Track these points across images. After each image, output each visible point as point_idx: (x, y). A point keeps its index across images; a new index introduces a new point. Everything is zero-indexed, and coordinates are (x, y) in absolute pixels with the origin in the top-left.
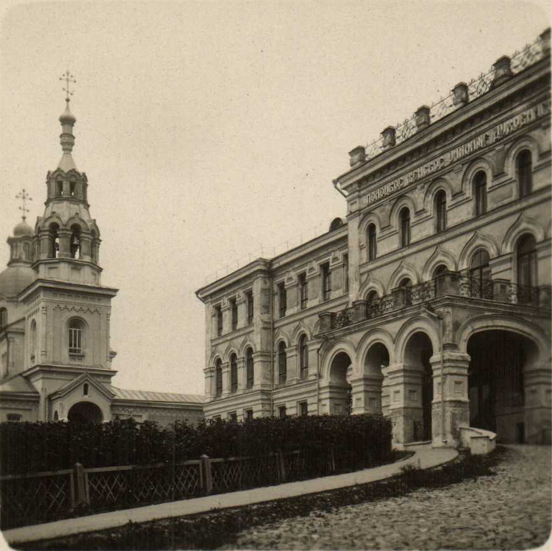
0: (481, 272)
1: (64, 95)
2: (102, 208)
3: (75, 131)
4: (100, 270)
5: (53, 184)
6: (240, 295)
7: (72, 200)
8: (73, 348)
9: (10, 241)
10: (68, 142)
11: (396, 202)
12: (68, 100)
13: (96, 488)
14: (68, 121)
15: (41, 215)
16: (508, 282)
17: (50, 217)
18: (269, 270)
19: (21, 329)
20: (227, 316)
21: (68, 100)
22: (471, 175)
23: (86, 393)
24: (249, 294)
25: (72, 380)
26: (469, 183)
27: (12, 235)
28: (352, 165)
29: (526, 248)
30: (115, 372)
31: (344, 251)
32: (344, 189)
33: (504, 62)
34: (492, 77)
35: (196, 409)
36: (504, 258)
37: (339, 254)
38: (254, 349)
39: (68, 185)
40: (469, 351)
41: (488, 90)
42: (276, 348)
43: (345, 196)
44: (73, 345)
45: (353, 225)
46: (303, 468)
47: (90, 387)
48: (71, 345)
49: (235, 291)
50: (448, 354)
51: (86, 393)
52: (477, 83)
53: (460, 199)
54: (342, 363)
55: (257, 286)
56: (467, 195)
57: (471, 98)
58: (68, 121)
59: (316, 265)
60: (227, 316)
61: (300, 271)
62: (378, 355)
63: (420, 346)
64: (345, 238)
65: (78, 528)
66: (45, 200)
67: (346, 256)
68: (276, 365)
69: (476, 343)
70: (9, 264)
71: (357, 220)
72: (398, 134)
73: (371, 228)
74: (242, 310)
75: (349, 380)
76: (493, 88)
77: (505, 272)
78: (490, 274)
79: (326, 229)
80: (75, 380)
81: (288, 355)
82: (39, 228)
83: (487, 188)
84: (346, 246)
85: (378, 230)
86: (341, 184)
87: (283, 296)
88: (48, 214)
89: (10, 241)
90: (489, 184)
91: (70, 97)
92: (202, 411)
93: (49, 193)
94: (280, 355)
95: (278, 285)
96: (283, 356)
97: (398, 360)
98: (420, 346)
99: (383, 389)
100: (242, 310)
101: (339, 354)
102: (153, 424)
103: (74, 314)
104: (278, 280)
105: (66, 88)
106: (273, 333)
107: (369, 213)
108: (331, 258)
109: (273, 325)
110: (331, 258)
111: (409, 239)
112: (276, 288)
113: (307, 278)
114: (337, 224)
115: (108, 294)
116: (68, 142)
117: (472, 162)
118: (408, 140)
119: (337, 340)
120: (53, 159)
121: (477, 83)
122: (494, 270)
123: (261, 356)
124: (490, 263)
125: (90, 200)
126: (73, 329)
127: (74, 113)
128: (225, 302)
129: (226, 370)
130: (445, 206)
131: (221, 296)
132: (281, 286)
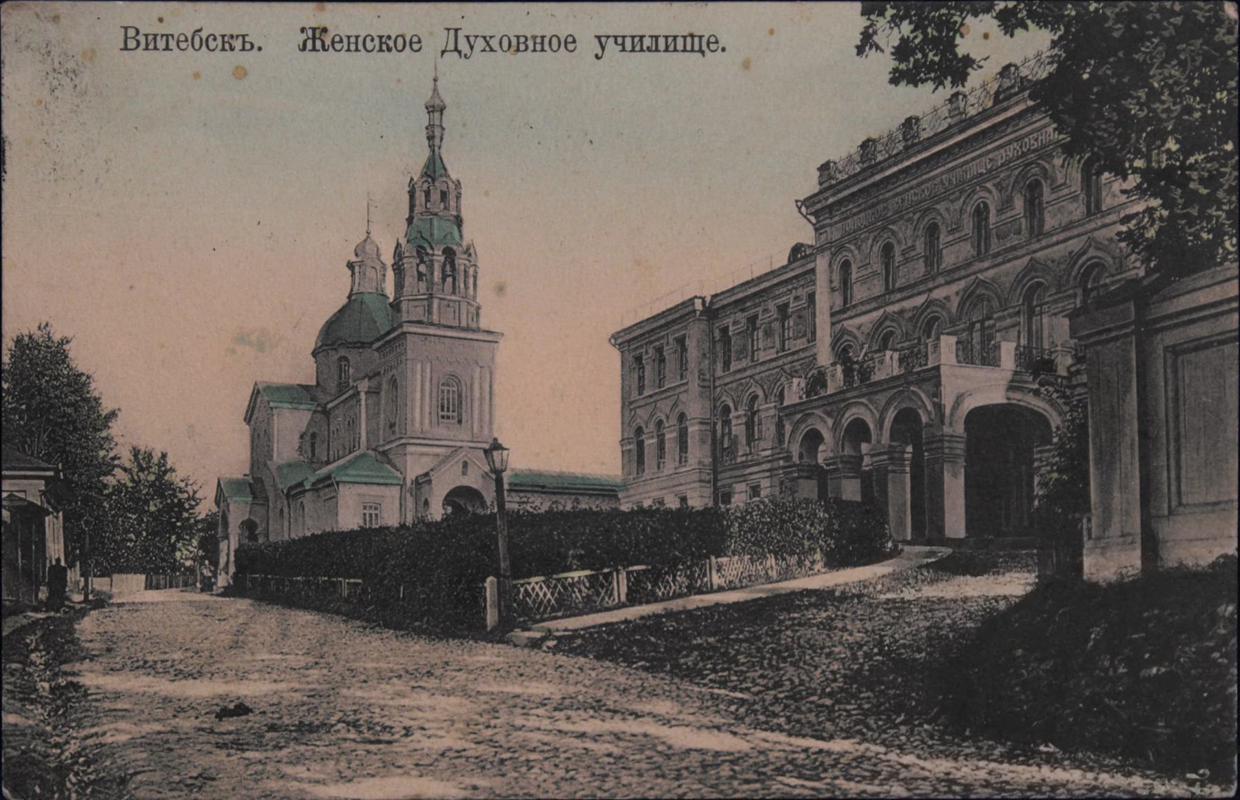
14: (435, 109)
18: (712, 311)
21: (435, 80)
22: (880, 243)
24: (681, 341)
26: (1079, 162)
28: (821, 184)
31: (808, 290)
32: (811, 214)
35: (608, 491)
37: (803, 292)
45: (821, 263)
46: (853, 247)
49: (686, 327)
52: (978, 93)
53: (957, 235)
56: (918, 250)
59: (772, 306)
61: (780, 301)
64: (813, 271)
65: (833, 290)
67: (811, 297)
84: (813, 282)
85: (854, 268)
86: (807, 207)
92: (616, 496)
107: (841, 248)
108: (791, 297)
110: (760, 309)
111: (894, 281)
112: (717, 334)
113: (790, 310)
114: (797, 251)
123: (701, 423)
129: (651, 441)
132: (725, 330)
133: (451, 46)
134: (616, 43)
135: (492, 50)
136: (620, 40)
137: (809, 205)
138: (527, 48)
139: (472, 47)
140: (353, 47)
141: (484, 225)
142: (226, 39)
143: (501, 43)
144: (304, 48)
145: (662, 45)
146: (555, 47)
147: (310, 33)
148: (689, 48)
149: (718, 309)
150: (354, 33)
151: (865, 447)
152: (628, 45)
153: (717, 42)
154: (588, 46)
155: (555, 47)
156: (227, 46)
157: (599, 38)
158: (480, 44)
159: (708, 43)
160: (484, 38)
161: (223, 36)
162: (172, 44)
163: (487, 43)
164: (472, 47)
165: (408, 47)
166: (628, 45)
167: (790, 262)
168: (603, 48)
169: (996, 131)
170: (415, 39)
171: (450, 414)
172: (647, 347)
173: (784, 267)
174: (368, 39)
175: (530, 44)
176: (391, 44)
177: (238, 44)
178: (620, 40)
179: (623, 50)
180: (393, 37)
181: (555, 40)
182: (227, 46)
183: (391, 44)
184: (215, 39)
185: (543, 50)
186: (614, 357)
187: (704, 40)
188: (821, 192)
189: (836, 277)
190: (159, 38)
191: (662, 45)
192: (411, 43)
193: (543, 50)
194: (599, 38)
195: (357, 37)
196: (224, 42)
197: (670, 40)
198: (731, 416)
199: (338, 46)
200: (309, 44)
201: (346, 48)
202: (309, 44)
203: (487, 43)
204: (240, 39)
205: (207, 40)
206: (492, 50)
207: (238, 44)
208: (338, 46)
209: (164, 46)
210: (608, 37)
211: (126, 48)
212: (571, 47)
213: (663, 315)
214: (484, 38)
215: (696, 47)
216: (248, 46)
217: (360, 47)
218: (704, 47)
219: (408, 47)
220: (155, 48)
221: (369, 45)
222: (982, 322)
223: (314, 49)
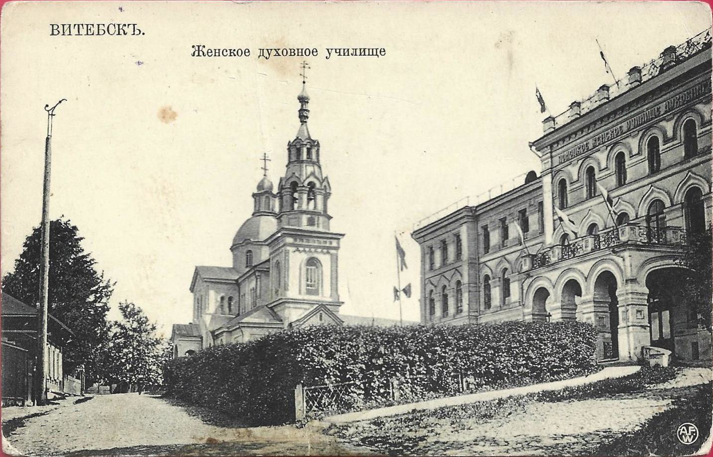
0: (657, 217)
2: (332, 163)
3: (309, 106)
4: (330, 218)
5: (294, 151)
6: (450, 238)
7: (310, 161)
8: (309, 283)
10: (303, 116)
12: (304, 82)
13: (311, 403)
15: (283, 175)
17: (291, 177)
18: (473, 214)
19: (267, 268)
20: (438, 255)
24: (458, 237)
27: (256, 191)
29: (693, 202)
33: (671, 50)
34: (661, 62)
36: (676, 207)
39: (302, 150)
40: (648, 285)
41: (657, 74)
44: (309, 280)
45: (547, 180)
48: (307, 281)
50: (629, 287)
51: (321, 319)
54: (542, 294)
57: (644, 79)
58: (303, 100)
60: (438, 255)
63: (607, 281)
68: (482, 293)
69: (653, 280)
72: (644, 72)
74: (452, 249)
77: (677, 220)
78: (666, 220)
79: (521, 181)
83: (660, 150)
88: (290, 174)
89: (254, 195)
93: (290, 157)
94: (485, 286)
96: (487, 287)
97: (589, 291)
98: (607, 281)
100: (452, 249)
102: (237, 344)
104: (481, 224)
105: (302, 74)
108: (528, 205)
112: (481, 231)
115: (338, 237)
116: (303, 116)
117: (648, 128)
118: (591, 111)
120: (291, 130)
121: (649, 67)
122: (668, 217)
124: (665, 211)
125: (322, 162)
126: (309, 267)
127: (309, 93)
128: (436, 243)
130: (624, 165)
131: (435, 236)
134: (336, 52)
135: (279, 55)
136: (338, 52)
138: (295, 54)
139: (269, 54)
140: (217, 54)
142: (232, 51)
144: (194, 55)
145: (358, 53)
146: (307, 54)
147: (197, 48)
148: (371, 54)
151: (577, 299)
152: (342, 53)
154: (323, 53)
155: (307, 54)
157: (328, 50)
158: (274, 52)
159: (380, 52)
160: (275, 50)
161: (230, 50)
165: (243, 54)
166: (342, 53)
170: (315, 50)
174: (225, 51)
175: (296, 52)
176: (235, 53)
177: (129, 30)
178: (338, 51)
179: (340, 55)
180: (236, 51)
181: (307, 51)
183: (235, 53)
184: (226, 51)
185: (302, 55)
187: (378, 51)
188: (545, 136)
189: (557, 189)
191: (358, 53)
192: (313, 52)
193: (302, 55)
194: (328, 50)
195: (302, 49)
197: (363, 54)
199: (210, 54)
200: (196, 53)
201: (214, 54)
202: (196, 53)
204: (131, 26)
205: (310, 53)
206: (279, 55)
207: (129, 30)
210: (271, 50)
214: (275, 50)
215: (375, 53)
218: (378, 53)
219: (243, 54)
221: (225, 53)
222: (657, 215)
223: (199, 55)
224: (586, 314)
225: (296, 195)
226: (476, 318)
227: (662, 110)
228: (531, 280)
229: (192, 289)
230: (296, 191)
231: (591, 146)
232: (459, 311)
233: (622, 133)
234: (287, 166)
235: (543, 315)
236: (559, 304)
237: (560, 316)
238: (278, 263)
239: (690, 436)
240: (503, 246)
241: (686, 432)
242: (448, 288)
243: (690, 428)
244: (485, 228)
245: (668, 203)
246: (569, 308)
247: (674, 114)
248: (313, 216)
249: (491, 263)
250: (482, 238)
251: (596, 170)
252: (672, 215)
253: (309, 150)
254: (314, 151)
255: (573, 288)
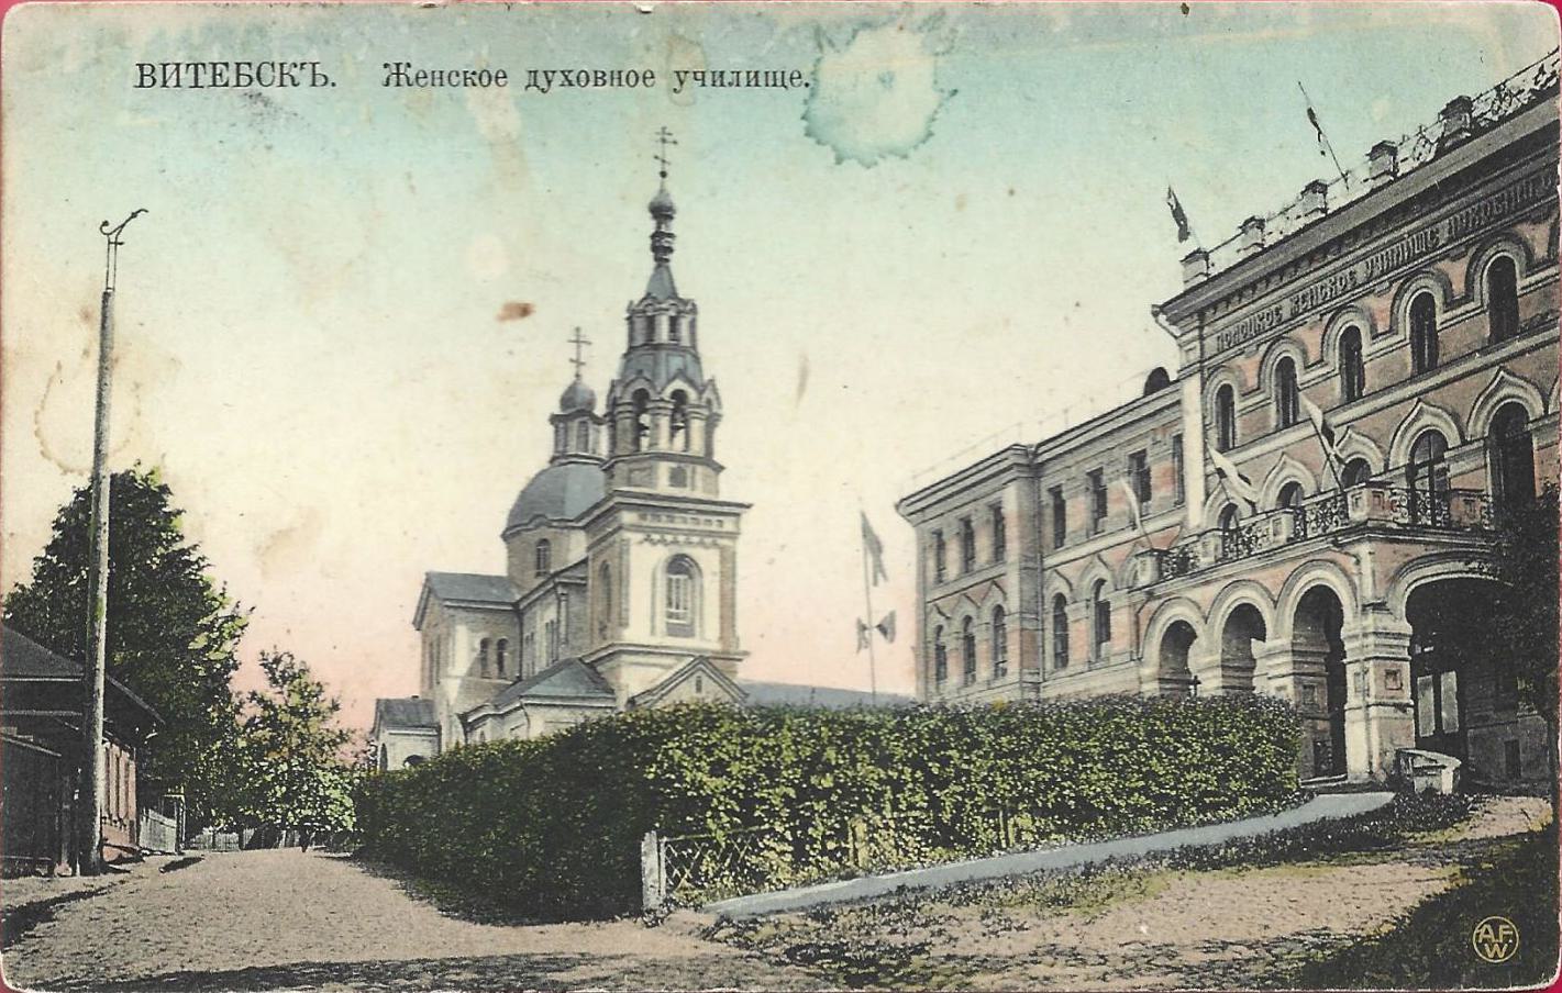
0: (1431, 470)
1: (658, 167)
3: (675, 226)
5: (640, 324)
8: (673, 610)
9: (554, 419)
10: (661, 248)
11: (1269, 348)
12: (663, 174)
16: (1478, 494)
18: (1031, 463)
19: (582, 579)
22: (1407, 302)
23: (699, 689)
25: (670, 667)
27: (558, 411)
30: (746, 653)
38: (1006, 609)
42: (1049, 606)
43: (1176, 337)
45: (1192, 387)
47: (705, 680)
48: (670, 604)
50: (1370, 621)
51: (699, 689)
55: (1012, 499)
61: (1132, 449)
62: (1246, 623)
63: (1320, 610)
66: (624, 351)
70: (553, 460)
71: (1195, 382)
73: (1225, 393)
74: (983, 544)
75: (1192, 665)
76: (1440, 153)
77: (1471, 473)
78: (1449, 474)
79: (1135, 389)
80: (681, 666)
81: (1071, 618)
82: (615, 398)
87: (1060, 509)
89: (554, 419)
90: (1238, 406)
91: (667, 168)
93: (631, 338)
94: (1055, 617)
95: (1050, 490)
97: (1281, 629)
98: (1320, 610)
99: (1255, 682)
101: (1172, 625)
103: (676, 550)
104: (1048, 482)
105: (659, 155)
106: (1043, 577)
109: (1042, 562)
112: (1047, 498)
114: (1157, 380)
115: (737, 509)
116: (661, 248)
118: (1287, 238)
119: (1171, 599)
121: (1413, 142)
122: (1454, 469)
124: (1446, 455)
126: (674, 577)
133: (532, 82)
135: (571, 84)
137: (1170, 311)
139: (549, 82)
141: (723, 348)
142: (468, 75)
143: (578, 78)
145: (743, 81)
149: (1042, 464)
150: (616, 69)
151: (1257, 647)
152: (708, 81)
153: (800, 77)
156: (287, 80)
160: (563, 72)
162: (206, 79)
163: (566, 77)
164: (549, 82)
165: (640, 82)
167: (1146, 393)
168: (682, 83)
169: (1389, 221)
171: (681, 611)
172: (954, 515)
173: (1131, 407)
181: (485, 75)
182: (287, 80)
186: (424, 577)
188: (1186, 293)
190: (183, 68)
192: (497, 78)
196: (466, 79)
198: (1067, 609)
199: (422, 82)
203: (566, 77)
208: (422, 82)
209: (175, 83)
211: (142, 85)
212: (501, 81)
213: (962, 475)
216: (699, 76)
217: (624, 83)
220: (757, 85)
222: (1430, 464)
224: (1275, 677)
225: (645, 419)
226: (1036, 687)
227: (1443, 236)
228: (1155, 604)
229: (418, 624)
230: (645, 411)
231: (1286, 314)
232: (999, 671)
233: (1280, 322)
234: (625, 355)
235: (1179, 679)
236: (1218, 658)
237: (1218, 682)
238: (605, 568)
239: (1501, 946)
240: (1095, 530)
241: (1491, 935)
242: (975, 621)
243: (1501, 927)
244: (1056, 492)
245: (1453, 439)
246: (1240, 667)
247: (1468, 245)
248: (683, 464)
249: (1072, 566)
250: (1049, 513)
251: (1298, 367)
252: (1464, 465)
253: (674, 322)
254: (684, 323)
255: (1246, 623)
